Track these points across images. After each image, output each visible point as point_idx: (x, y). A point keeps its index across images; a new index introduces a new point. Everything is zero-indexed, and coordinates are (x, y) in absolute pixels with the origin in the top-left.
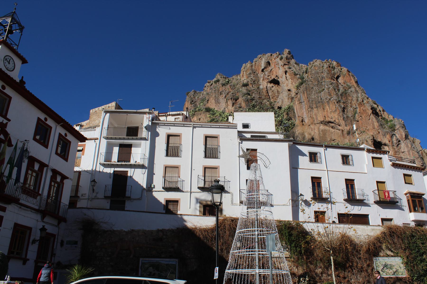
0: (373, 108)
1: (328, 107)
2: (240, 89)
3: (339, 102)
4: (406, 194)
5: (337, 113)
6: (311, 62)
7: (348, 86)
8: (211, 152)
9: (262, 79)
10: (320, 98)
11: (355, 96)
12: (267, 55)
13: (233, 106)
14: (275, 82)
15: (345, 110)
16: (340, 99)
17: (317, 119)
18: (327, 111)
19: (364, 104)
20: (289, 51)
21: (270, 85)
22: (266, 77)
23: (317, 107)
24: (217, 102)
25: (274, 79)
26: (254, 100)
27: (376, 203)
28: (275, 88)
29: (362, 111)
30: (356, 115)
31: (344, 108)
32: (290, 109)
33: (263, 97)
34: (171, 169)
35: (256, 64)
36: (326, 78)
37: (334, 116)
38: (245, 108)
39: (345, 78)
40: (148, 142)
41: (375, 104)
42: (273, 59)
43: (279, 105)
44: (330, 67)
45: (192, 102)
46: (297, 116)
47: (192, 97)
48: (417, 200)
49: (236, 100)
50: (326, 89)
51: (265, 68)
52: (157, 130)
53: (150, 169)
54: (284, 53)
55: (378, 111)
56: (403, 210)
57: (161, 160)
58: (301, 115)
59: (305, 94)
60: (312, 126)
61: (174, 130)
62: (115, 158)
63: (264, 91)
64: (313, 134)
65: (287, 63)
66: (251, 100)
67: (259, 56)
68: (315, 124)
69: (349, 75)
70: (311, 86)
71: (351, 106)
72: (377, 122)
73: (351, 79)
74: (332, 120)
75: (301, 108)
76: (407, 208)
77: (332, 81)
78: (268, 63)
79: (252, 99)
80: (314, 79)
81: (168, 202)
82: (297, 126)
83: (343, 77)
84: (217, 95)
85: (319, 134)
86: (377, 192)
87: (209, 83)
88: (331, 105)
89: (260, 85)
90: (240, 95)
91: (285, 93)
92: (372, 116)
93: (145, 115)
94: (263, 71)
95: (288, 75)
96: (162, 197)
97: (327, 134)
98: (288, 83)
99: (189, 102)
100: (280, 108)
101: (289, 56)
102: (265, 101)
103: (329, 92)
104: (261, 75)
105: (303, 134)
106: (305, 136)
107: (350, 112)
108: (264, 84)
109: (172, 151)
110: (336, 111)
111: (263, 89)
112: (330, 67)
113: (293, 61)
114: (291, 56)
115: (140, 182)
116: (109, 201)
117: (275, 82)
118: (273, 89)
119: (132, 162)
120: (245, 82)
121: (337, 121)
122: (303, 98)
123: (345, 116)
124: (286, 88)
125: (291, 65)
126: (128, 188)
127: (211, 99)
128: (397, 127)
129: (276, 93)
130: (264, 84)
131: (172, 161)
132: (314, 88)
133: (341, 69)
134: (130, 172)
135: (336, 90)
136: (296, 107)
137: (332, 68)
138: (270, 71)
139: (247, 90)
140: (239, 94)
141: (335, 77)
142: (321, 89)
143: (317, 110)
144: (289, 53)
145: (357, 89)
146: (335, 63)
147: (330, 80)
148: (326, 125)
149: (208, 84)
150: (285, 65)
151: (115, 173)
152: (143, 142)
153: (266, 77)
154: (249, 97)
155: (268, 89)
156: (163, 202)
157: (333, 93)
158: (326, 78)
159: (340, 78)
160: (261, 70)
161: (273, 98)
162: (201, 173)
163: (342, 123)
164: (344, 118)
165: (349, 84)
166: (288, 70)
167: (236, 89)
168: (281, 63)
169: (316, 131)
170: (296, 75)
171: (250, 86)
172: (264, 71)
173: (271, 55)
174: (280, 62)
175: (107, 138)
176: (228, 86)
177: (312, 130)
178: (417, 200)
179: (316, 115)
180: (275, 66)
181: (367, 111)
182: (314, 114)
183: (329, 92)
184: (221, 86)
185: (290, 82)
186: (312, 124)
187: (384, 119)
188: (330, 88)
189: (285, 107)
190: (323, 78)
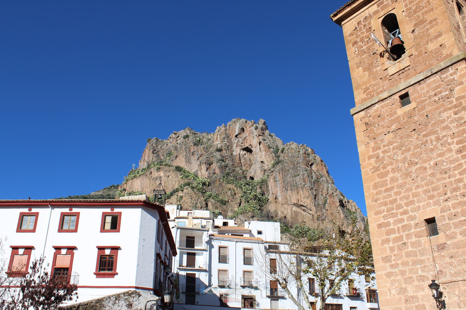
0: (341, 201)
1: (302, 192)
2: (214, 154)
3: (312, 189)
4: (366, 290)
5: (310, 199)
6: (288, 144)
7: (320, 175)
8: (247, 261)
9: (235, 145)
10: (295, 182)
11: (326, 185)
12: (241, 121)
13: (207, 170)
14: (248, 150)
15: (317, 197)
16: (313, 186)
17: (291, 200)
18: (301, 196)
19: (334, 196)
20: (264, 122)
21: (243, 152)
22: (240, 143)
23: (291, 190)
24: (188, 161)
25: (248, 147)
26: (227, 167)
27: (348, 296)
28: (248, 155)
29: (331, 202)
30: (326, 205)
31: (316, 195)
32: (264, 183)
33: (236, 165)
34: (222, 272)
35: (230, 128)
36: (301, 163)
37: (307, 202)
38: (219, 174)
39: (318, 166)
40: (208, 253)
41: (342, 195)
42: (248, 127)
43: (252, 175)
44: (305, 153)
45: (154, 151)
46: (271, 192)
47: (154, 145)
48: (372, 294)
49: (210, 165)
50: (301, 175)
51: (239, 134)
52: (212, 243)
53: (209, 271)
54: (260, 123)
55: (344, 202)
56: (364, 301)
57: (216, 266)
58: (275, 193)
59: (281, 174)
60: (285, 206)
61: (223, 243)
62: (185, 263)
63: (237, 158)
64: (285, 213)
65: (262, 134)
66: (225, 167)
67: (234, 120)
68: (288, 205)
69: (322, 164)
70: (287, 168)
71: (322, 195)
72: (343, 214)
73: (323, 168)
74: (305, 205)
75: (276, 186)
76: (365, 300)
77: (307, 168)
78: (243, 130)
79: (226, 166)
80: (290, 162)
81: (221, 295)
82: (271, 202)
83: (317, 165)
84: (188, 154)
85: (292, 214)
86: (348, 289)
87: (175, 134)
88: (305, 191)
89: (233, 151)
90: (214, 160)
91: (258, 165)
92: (339, 208)
93: (204, 232)
94: (236, 136)
95: (261, 146)
96: (218, 292)
97: (299, 216)
98: (261, 156)
99: (151, 151)
100: (252, 178)
101: (264, 126)
102: (238, 169)
103: (304, 179)
104: (235, 141)
105: (276, 211)
106: (278, 213)
107: (321, 199)
108: (237, 151)
109: (223, 259)
110: (308, 197)
111: (236, 156)
112: (305, 153)
113: (267, 132)
114: (266, 127)
115: (205, 283)
116: (185, 295)
117: (248, 150)
118: (245, 156)
119: (197, 267)
120: (219, 146)
121: (309, 206)
122: (279, 177)
123: (316, 203)
124: (260, 160)
125: (265, 136)
126: (196, 287)
127: (181, 156)
128: (359, 220)
129: (248, 161)
130: (237, 151)
131: (223, 266)
132: (290, 171)
133: (315, 157)
134: (197, 275)
135: (310, 177)
136: (271, 183)
137: (307, 155)
138: (244, 138)
139: (221, 155)
140: (213, 159)
141: (310, 164)
142: (296, 174)
143: (292, 192)
144: (264, 124)
145: (328, 179)
146: (310, 150)
147: (305, 166)
148: (298, 207)
149: (174, 136)
150: (260, 135)
151: (188, 275)
152: (204, 252)
153: (240, 143)
154: (223, 163)
155: (241, 156)
156: (218, 295)
157: (307, 179)
158: (301, 163)
159: (314, 165)
160: (235, 135)
161: (244, 166)
162: (242, 276)
163: (314, 209)
164: (315, 205)
165: (321, 172)
166: (262, 141)
167: (210, 152)
168: (256, 133)
169: (289, 211)
170: (270, 148)
171: (224, 151)
172: (238, 136)
173: (246, 121)
174: (255, 131)
175: (180, 249)
176: (202, 146)
177: (285, 210)
178: (372, 294)
179: (289, 196)
180: (249, 134)
181: (336, 203)
182: (288, 195)
183: (304, 179)
184: (193, 145)
185: (264, 154)
186: (286, 204)
187: (348, 209)
188: (305, 174)
189: (257, 179)
190: (298, 163)
